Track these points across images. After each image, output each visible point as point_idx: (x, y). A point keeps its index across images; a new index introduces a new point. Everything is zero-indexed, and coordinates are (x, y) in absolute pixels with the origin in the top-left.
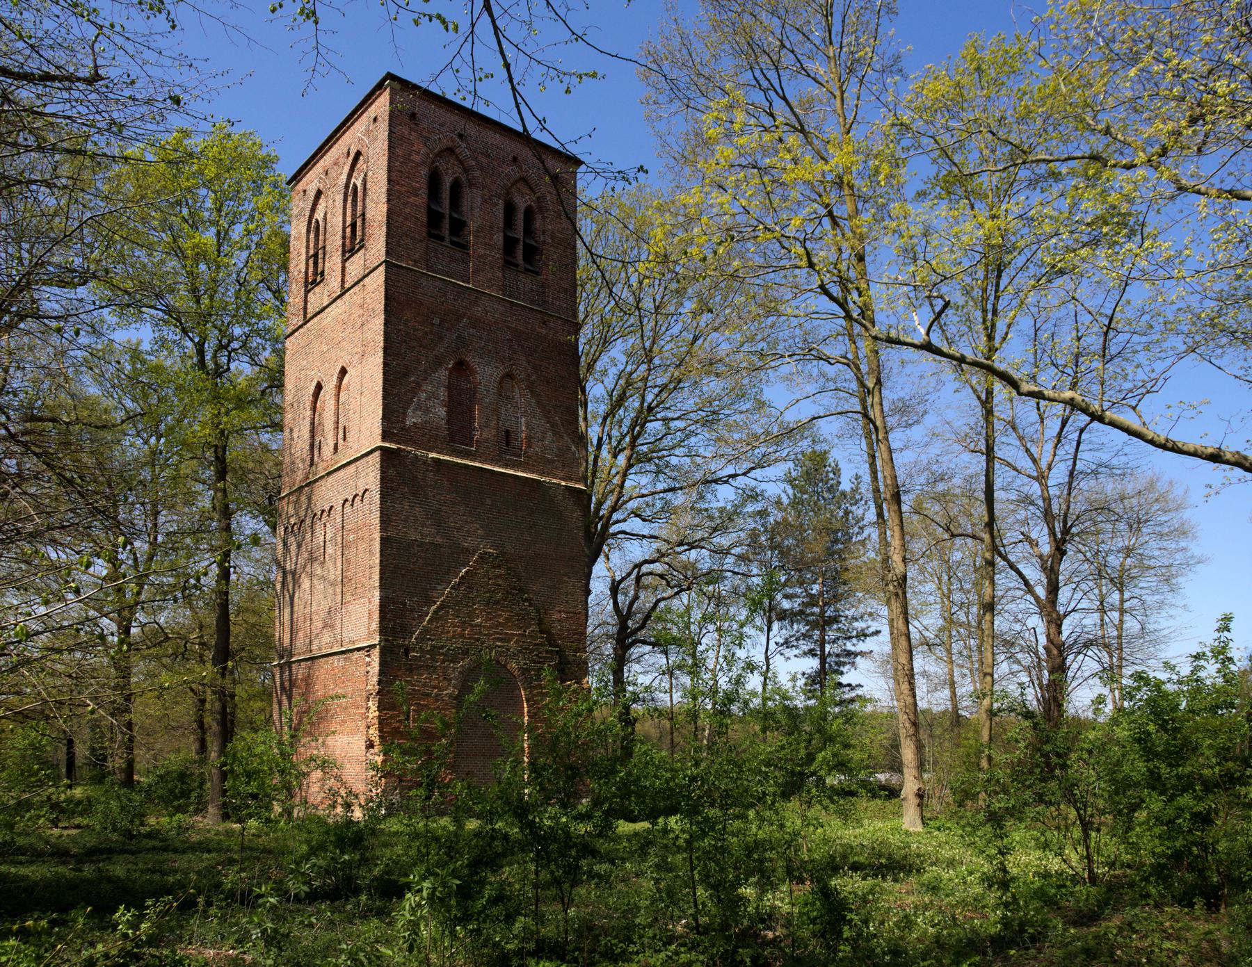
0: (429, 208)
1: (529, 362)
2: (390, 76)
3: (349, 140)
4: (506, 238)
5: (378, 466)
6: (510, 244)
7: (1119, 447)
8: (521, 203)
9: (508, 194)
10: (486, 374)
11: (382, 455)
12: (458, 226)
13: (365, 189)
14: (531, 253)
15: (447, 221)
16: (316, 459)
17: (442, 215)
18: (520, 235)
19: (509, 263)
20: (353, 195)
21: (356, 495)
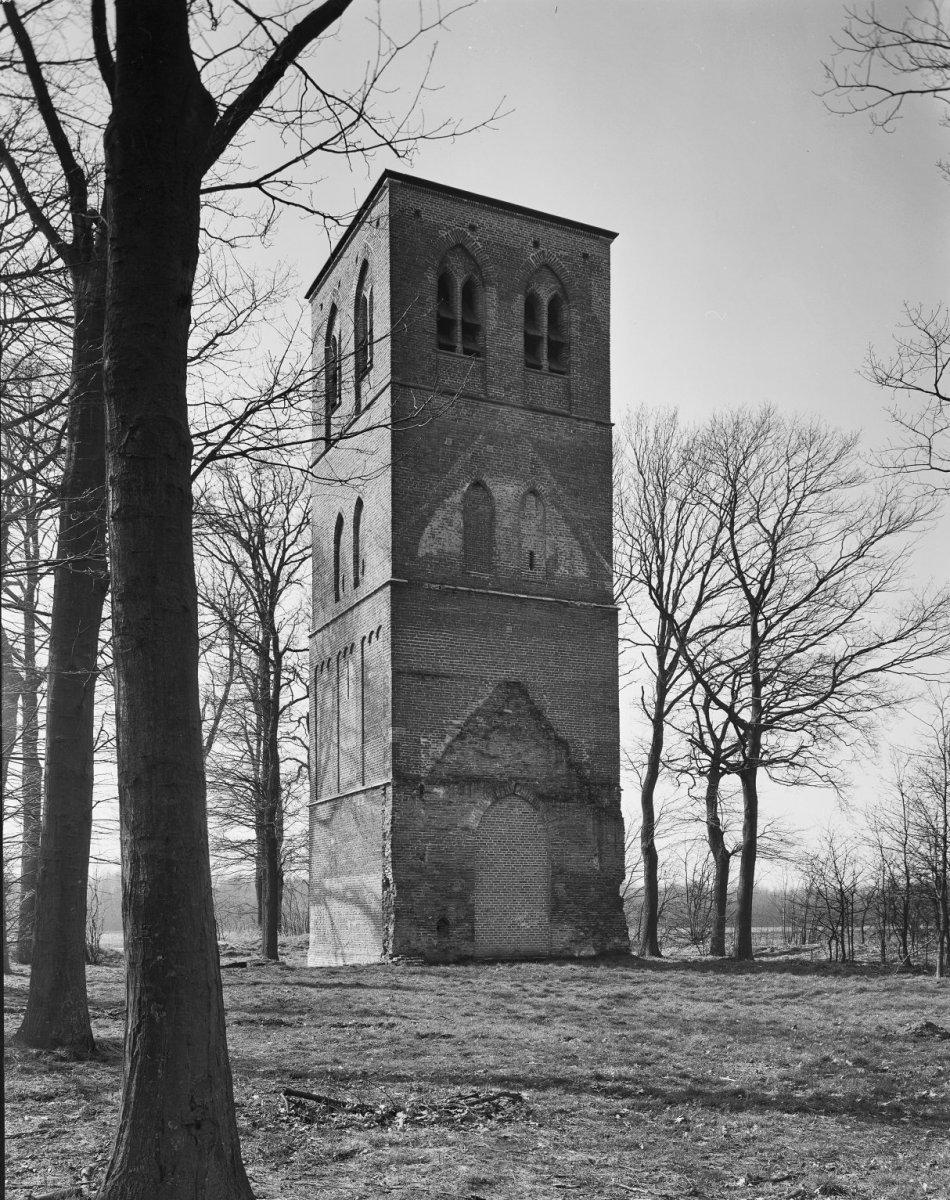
0: (438, 315)
1: (553, 475)
2: (388, 173)
3: (355, 248)
4: (527, 336)
5: (389, 601)
6: (531, 344)
7: (34, 133)
8: (545, 295)
9: (444, 261)
10: (505, 491)
11: (392, 590)
12: (472, 331)
13: (371, 302)
14: (557, 350)
15: (545, 341)
16: (341, 594)
17: (541, 338)
18: (544, 331)
19: (532, 364)
20: (362, 307)
21: (372, 633)
